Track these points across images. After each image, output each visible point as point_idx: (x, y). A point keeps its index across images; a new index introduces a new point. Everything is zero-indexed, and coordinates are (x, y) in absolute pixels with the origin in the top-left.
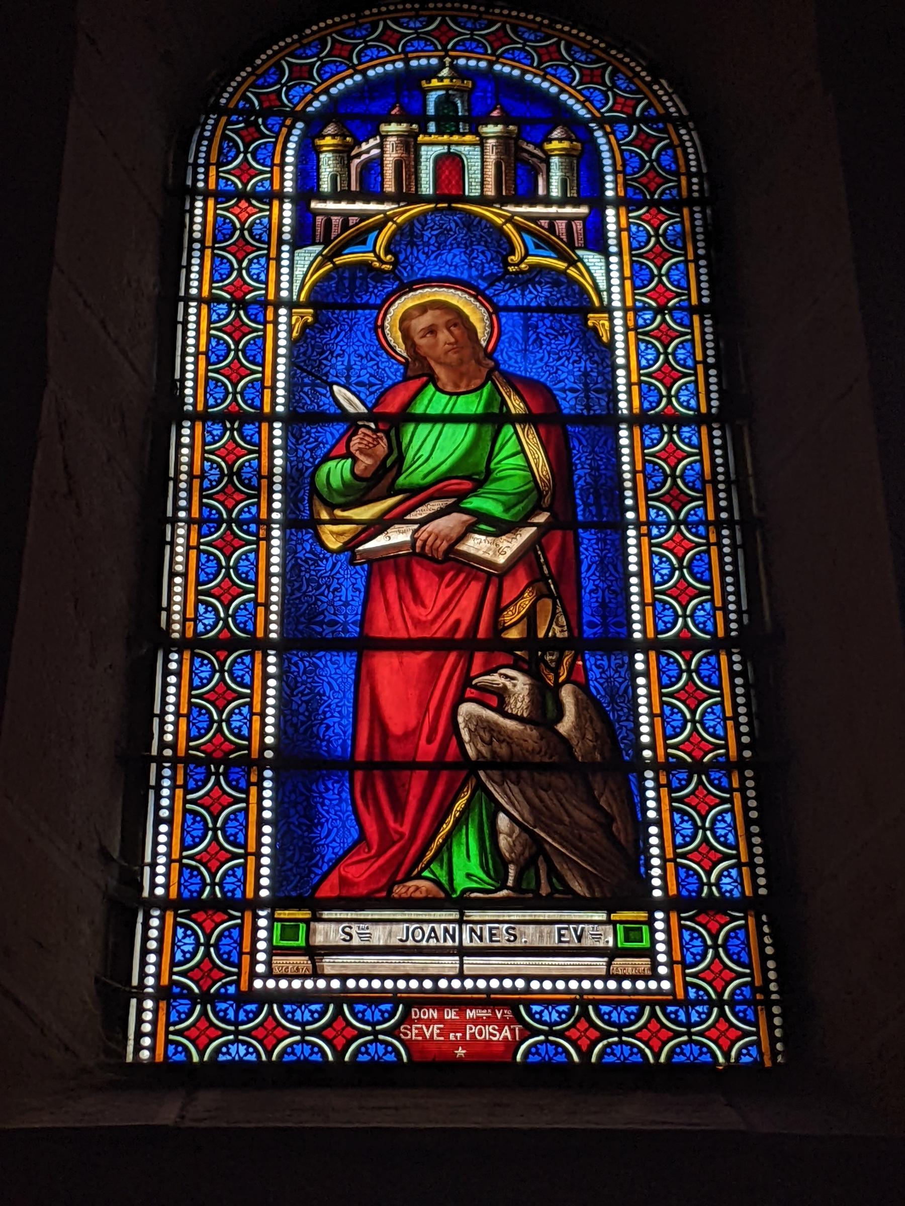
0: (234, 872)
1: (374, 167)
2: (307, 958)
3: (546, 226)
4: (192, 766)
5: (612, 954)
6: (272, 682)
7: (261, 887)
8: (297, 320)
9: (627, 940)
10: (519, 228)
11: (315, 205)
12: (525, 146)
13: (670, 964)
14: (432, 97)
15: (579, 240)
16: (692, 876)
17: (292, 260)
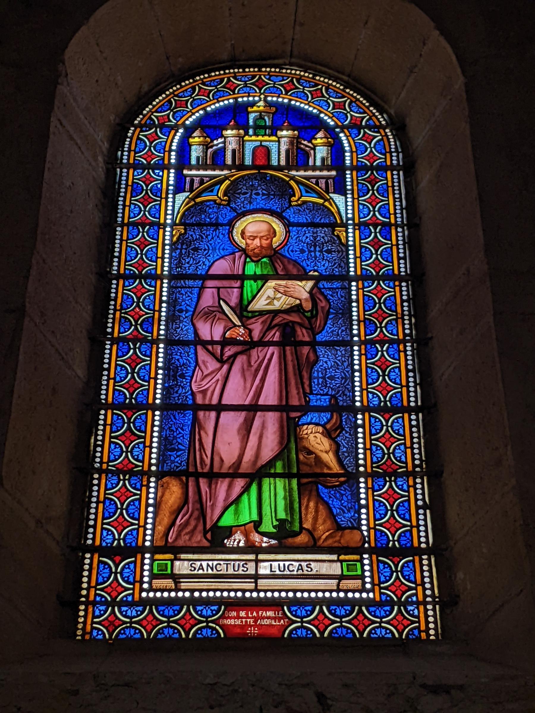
0: (145, 367)
1: (221, 153)
2: (171, 580)
3: (314, 182)
4: (110, 475)
5: (341, 578)
6: (164, 305)
7: (152, 458)
8: (176, 232)
9: (348, 571)
10: (298, 182)
11: (185, 172)
12: (303, 142)
13: (372, 583)
14: (252, 117)
15: (331, 189)
16: (384, 536)
17: (174, 198)
